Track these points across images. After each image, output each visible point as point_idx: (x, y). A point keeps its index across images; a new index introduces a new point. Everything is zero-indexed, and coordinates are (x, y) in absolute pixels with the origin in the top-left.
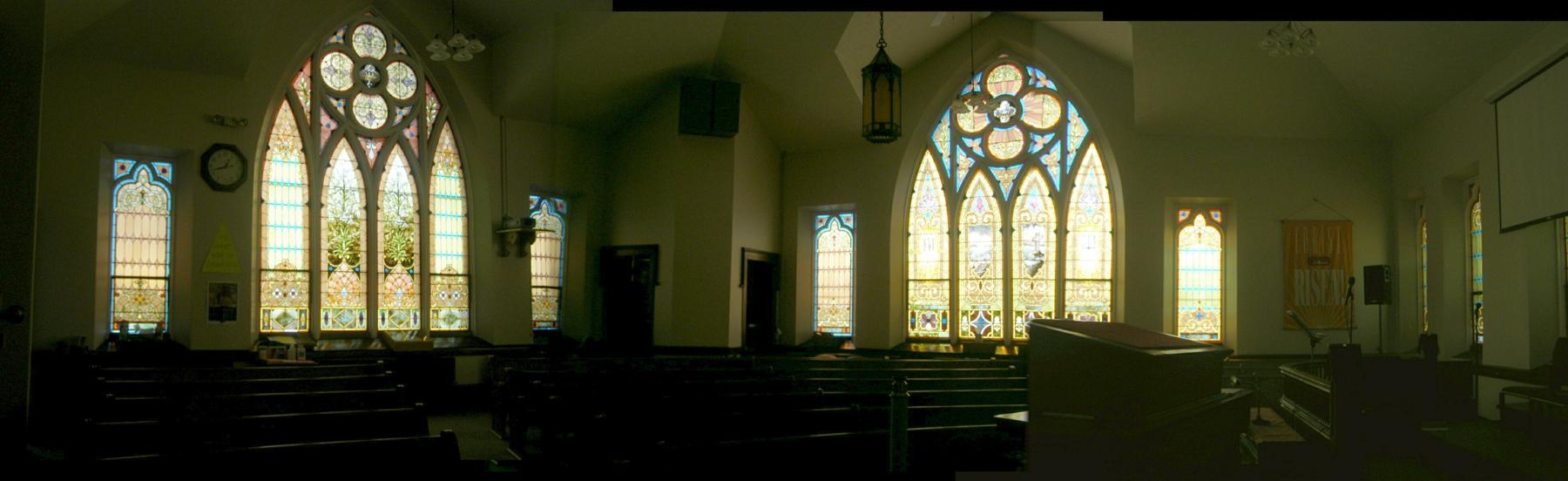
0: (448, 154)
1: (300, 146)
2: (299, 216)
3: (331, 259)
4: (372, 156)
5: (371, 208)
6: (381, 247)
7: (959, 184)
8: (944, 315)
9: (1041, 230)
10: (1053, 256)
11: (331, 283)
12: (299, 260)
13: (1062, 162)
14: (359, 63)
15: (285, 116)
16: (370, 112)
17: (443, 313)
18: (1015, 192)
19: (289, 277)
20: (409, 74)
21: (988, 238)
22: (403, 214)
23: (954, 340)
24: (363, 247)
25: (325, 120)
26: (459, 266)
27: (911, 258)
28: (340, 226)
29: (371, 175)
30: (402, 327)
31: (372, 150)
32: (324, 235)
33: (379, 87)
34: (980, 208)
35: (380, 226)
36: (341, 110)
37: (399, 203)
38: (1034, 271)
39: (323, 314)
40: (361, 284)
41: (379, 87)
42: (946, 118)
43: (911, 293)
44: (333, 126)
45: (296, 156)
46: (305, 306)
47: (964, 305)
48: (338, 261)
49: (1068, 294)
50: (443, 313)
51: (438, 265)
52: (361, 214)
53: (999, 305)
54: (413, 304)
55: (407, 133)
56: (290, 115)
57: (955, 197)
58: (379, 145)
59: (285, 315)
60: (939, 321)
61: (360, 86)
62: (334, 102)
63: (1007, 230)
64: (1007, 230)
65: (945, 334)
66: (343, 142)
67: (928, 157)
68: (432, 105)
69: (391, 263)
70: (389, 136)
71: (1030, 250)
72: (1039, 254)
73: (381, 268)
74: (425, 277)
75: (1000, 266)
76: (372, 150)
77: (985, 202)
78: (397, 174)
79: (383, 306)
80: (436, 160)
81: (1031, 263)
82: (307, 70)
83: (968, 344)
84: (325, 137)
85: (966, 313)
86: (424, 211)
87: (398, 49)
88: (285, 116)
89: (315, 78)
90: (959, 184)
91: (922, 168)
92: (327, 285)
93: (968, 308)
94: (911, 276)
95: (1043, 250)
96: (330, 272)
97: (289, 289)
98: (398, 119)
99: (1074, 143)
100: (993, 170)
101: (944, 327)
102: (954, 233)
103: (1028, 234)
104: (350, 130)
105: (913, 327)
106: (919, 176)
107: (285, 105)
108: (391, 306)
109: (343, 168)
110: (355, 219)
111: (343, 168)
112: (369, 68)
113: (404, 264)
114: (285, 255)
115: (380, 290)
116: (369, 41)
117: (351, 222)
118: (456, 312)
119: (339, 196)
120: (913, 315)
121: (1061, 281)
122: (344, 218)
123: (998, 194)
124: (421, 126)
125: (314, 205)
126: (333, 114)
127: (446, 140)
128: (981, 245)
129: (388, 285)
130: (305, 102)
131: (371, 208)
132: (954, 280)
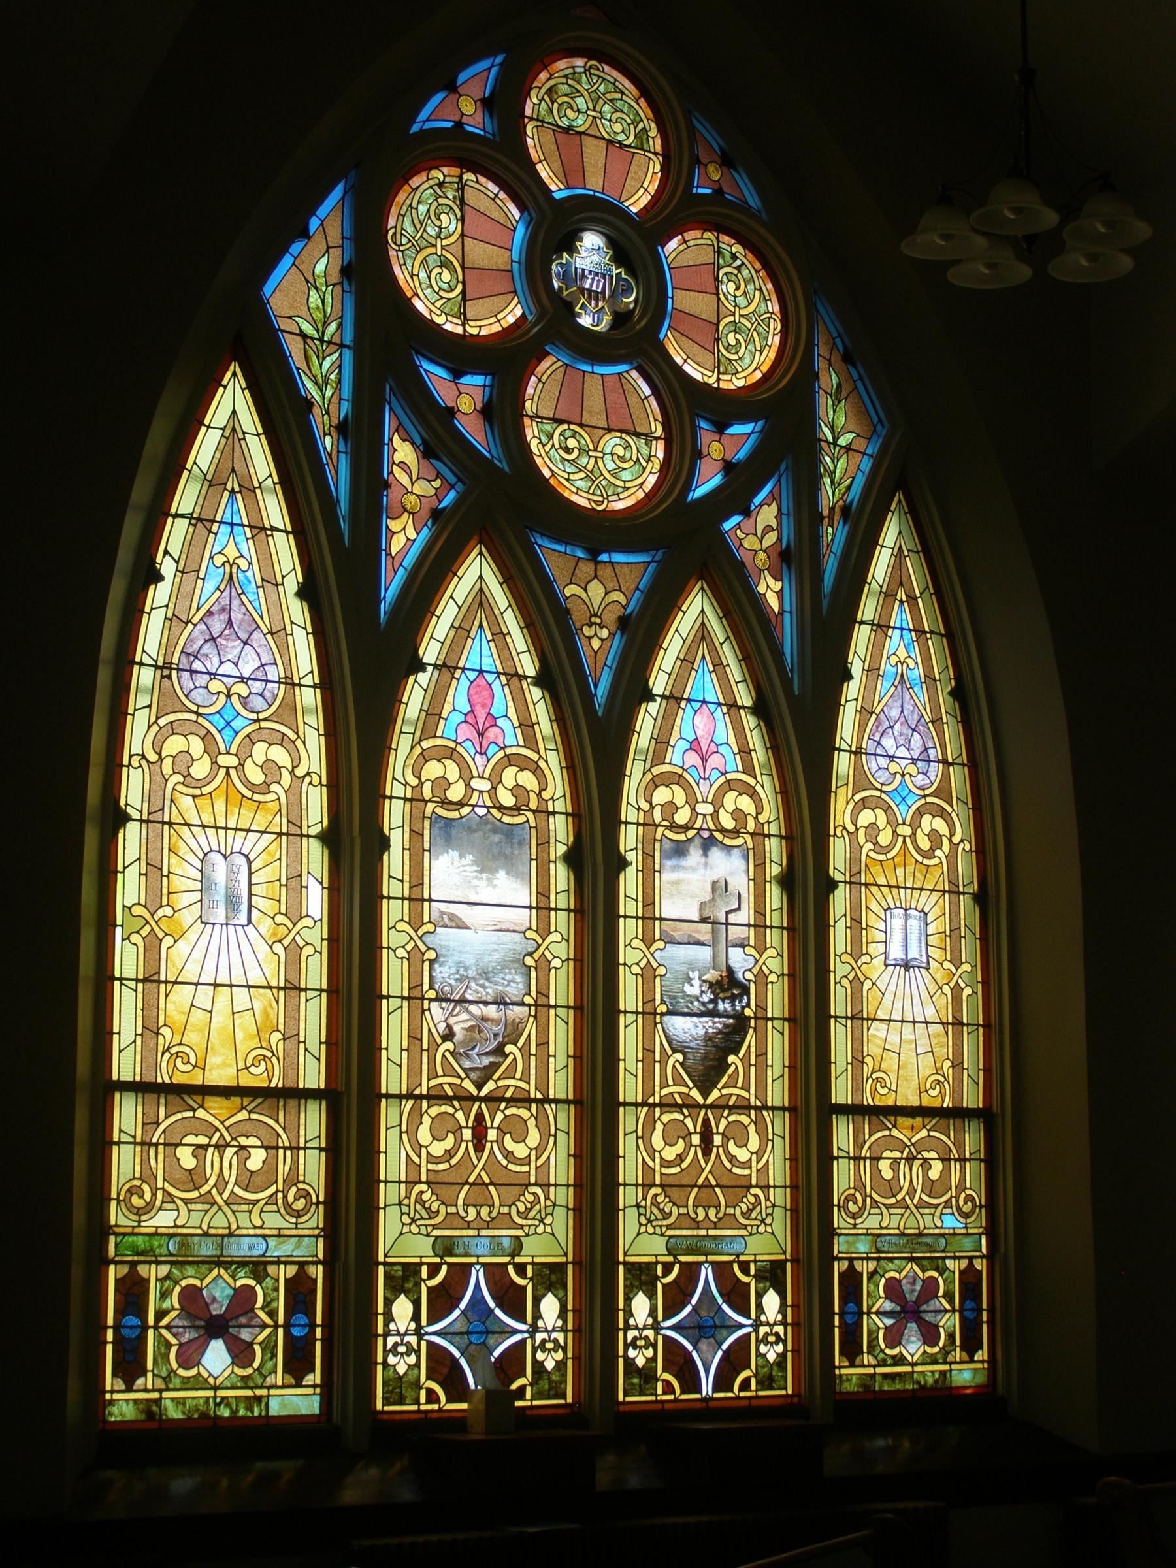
7: (391, 586)
8: (300, 1290)
9: (730, 867)
10: (776, 1001)
13: (796, 558)
18: (633, 689)
21: (512, 890)
23: (355, 1425)
27: (127, 959)
34: (481, 726)
38: (710, 1065)
42: (330, 215)
43: (124, 1164)
47: (399, 1237)
49: (842, 1176)
53: (550, 1238)
57: (368, 665)
60: (266, 1332)
63: (595, 862)
64: (595, 862)
65: (297, 1401)
67: (232, 401)
70: (678, 541)
71: (688, 964)
72: (728, 985)
75: (561, 1036)
77: (502, 703)
81: (689, 1028)
83: (420, 1441)
84: (404, 538)
85: (404, 1279)
87: (465, 108)
89: (368, 274)
90: (391, 586)
91: (205, 450)
93: (419, 1249)
94: (125, 1065)
95: (740, 960)
99: (843, 473)
100: (554, 556)
101: (297, 1365)
102: (353, 843)
103: (684, 888)
105: (131, 1366)
106: (187, 497)
112: (591, 251)
116: (597, 123)
120: (133, 1293)
121: (812, 1111)
123: (559, 674)
124: (805, 511)
126: (438, 438)
128: (477, 916)
130: (324, 380)
132: (351, 1100)
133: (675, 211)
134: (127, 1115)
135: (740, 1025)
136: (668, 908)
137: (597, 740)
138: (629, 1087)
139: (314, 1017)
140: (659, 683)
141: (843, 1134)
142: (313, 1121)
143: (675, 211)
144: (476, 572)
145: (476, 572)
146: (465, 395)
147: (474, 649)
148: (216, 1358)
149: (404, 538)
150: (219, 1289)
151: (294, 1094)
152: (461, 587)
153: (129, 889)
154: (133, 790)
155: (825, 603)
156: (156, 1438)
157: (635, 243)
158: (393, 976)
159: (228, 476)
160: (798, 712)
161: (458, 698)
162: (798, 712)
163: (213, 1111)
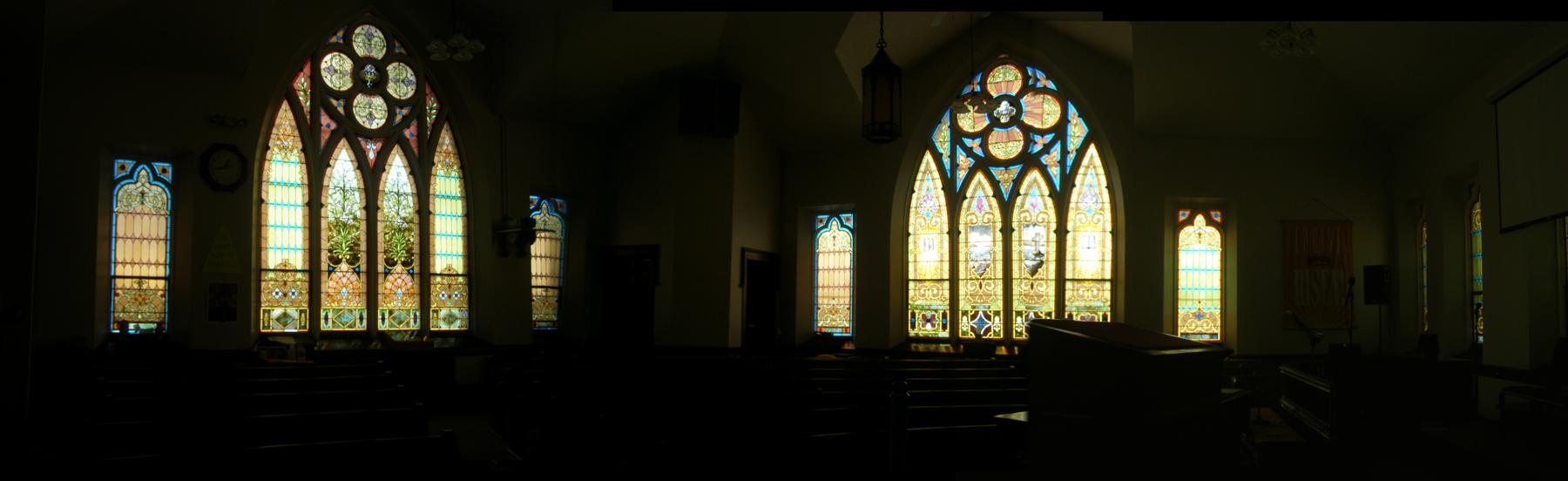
0: (448, 154)
1: (300, 146)
2: (298, 216)
3: (331, 259)
4: (372, 156)
5: (371, 208)
6: (381, 247)
8: (944, 315)
9: (1041, 230)
10: (1053, 256)
11: (331, 283)
12: (298, 260)
13: (1062, 163)
14: (359, 63)
15: (285, 117)
16: (371, 112)
17: (443, 313)
19: (289, 277)
20: (409, 74)
21: (988, 238)
22: (402, 214)
23: (372, 334)
24: (363, 247)
25: (325, 120)
26: (459, 265)
27: (911, 258)
28: (340, 226)
29: (371, 175)
30: (402, 327)
31: (372, 150)
32: (324, 234)
33: (379, 87)
34: (980, 208)
35: (380, 227)
36: (341, 110)
37: (399, 203)
38: (1034, 271)
39: (323, 314)
40: (360, 284)
41: (379, 87)
43: (911, 293)
44: (333, 126)
45: (296, 156)
46: (305, 306)
47: (963, 305)
48: (338, 261)
49: (1068, 294)
50: (443, 313)
51: (439, 265)
52: (360, 214)
53: (999, 305)
54: (413, 304)
55: (407, 133)
56: (290, 115)
57: (955, 197)
58: (379, 145)
59: (285, 315)
60: (939, 321)
61: (359, 86)
62: (334, 102)
63: (1007, 230)
64: (1007, 230)
65: (945, 334)
66: (343, 142)
67: (928, 157)
68: (432, 106)
69: (390, 263)
70: (389, 136)
71: (1030, 250)
72: (1039, 254)
73: (381, 268)
74: (425, 276)
75: (1000, 266)
76: (372, 150)
78: (397, 174)
79: (383, 306)
80: (436, 159)
81: (1031, 263)
82: (307, 70)
84: (325, 137)
85: (966, 313)
86: (424, 213)
87: (1044, 82)
88: (285, 117)
92: (328, 285)
93: (968, 308)
94: (911, 276)
95: (1043, 250)
96: (330, 273)
97: (290, 290)
98: (398, 118)
100: (993, 170)
101: (944, 327)
102: (954, 233)
103: (1028, 234)
104: (351, 131)
105: (913, 327)
106: (919, 176)
107: (285, 105)
108: (391, 306)
109: (343, 168)
110: (355, 219)
111: (343, 168)
113: (404, 264)
114: (286, 256)
115: (380, 290)
116: (369, 41)
117: (351, 222)
118: (455, 311)
119: (338, 196)
120: (913, 315)
121: (1061, 281)
122: (344, 218)
123: (998, 194)
124: (422, 126)
125: (314, 205)
126: (333, 114)
127: (446, 140)
128: (980, 245)
129: (388, 285)
131: (371, 208)
133: (388, 59)
134: (911, 285)
135: (1042, 262)
136: (1024, 237)
137: (1006, 208)
138: (962, 276)
139: (946, 266)
140: (1022, 191)
141: (1069, 285)
142: (946, 285)
143: (388, 59)
144: (979, 176)
145: (979, 176)
146: (975, 144)
147: (980, 192)
148: (929, 326)
149: (325, 137)
150: (929, 314)
151: (1104, 280)
152: (974, 182)
153: (911, 247)
154: (911, 230)
155: (414, 145)
156: (918, 339)
157: (1014, 101)
158: (962, 257)
159: (927, 170)
160: (1061, 198)
161: (975, 203)
162: (1061, 198)
163: (1086, 284)
